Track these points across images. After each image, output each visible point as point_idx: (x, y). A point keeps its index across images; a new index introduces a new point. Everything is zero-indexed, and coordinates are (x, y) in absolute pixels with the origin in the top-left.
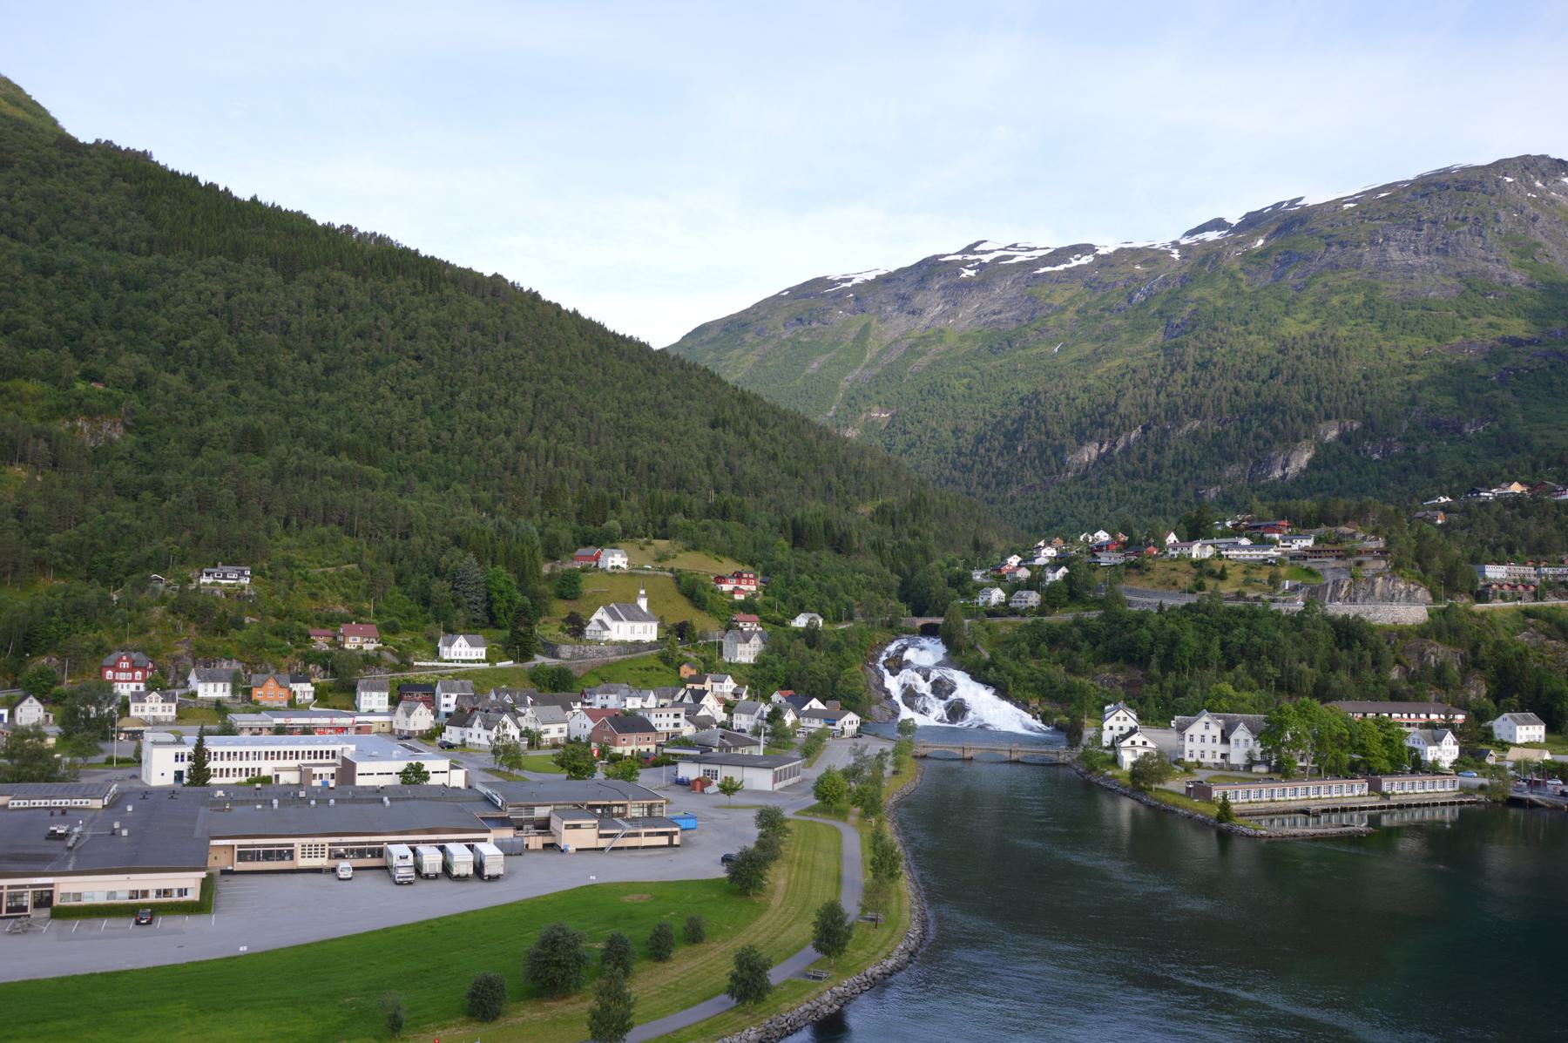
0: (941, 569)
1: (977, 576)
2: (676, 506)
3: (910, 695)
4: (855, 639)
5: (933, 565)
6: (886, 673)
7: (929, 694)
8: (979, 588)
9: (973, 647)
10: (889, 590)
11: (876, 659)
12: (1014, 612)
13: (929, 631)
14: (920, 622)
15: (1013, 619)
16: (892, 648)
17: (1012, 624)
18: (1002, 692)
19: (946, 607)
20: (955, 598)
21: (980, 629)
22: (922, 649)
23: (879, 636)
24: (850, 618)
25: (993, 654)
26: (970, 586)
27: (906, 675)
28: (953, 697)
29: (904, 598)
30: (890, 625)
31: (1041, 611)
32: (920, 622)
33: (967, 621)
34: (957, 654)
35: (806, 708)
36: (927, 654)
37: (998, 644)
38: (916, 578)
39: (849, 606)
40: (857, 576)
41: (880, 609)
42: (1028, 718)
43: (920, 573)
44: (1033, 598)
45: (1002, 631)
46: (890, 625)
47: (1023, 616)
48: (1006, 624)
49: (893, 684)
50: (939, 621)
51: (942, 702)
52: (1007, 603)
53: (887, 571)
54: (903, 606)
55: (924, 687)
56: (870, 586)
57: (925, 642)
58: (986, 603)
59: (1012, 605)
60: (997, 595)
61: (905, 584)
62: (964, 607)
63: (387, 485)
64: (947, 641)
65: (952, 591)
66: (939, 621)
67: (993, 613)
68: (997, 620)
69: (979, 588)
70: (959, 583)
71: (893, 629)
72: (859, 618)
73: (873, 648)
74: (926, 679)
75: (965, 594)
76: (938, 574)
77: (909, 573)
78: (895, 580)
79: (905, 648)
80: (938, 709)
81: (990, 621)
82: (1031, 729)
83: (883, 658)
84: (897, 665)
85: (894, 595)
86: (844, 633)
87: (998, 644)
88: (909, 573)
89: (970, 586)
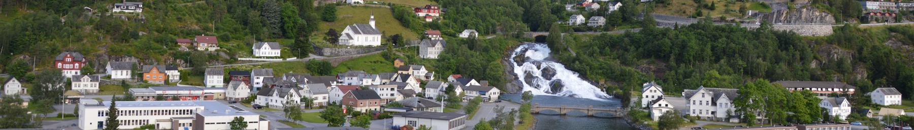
1: (569, 8)
3: (529, 77)
4: (497, 44)
6: (515, 64)
7: (540, 77)
8: (570, 15)
9: (566, 50)
10: (516, 16)
11: (509, 56)
12: (590, 29)
13: (540, 40)
14: (535, 34)
15: (589, 33)
16: (518, 50)
17: (589, 36)
18: (583, 76)
19: (550, 25)
20: (555, 21)
21: (571, 39)
22: (536, 50)
23: (511, 43)
24: (494, 32)
25: (577, 53)
26: (564, 14)
27: (527, 66)
28: (554, 78)
29: (526, 21)
30: (518, 37)
31: (606, 28)
32: (535, 34)
34: (557, 54)
35: (468, 85)
36: (539, 53)
38: (532, 9)
39: (493, 25)
40: (498, 8)
41: (511, 27)
42: (598, 90)
43: (535, 6)
44: (602, 21)
45: (583, 40)
46: (518, 37)
48: (586, 36)
49: (519, 71)
50: (546, 34)
51: (548, 82)
52: (586, 24)
53: (516, 5)
54: (525, 25)
55: (537, 73)
56: (506, 14)
57: (538, 46)
58: (574, 23)
60: (580, 19)
61: (526, 12)
62: (561, 26)
64: (551, 46)
66: (546, 34)
67: (577, 29)
68: (580, 34)
69: (570, 15)
70: (558, 11)
71: (519, 39)
72: (499, 32)
74: (539, 68)
75: (562, 18)
76: (545, 6)
77: (528, 6)
78: (521, 10)
79: (526, 50)
80: (545, 85)
81: (576, 34)
82: (600, 97)
83: (514, 56)
84: (521, 60)
85: (520, 19)
86: (491, 41)
88: (528, 6)
89: (564, 14)
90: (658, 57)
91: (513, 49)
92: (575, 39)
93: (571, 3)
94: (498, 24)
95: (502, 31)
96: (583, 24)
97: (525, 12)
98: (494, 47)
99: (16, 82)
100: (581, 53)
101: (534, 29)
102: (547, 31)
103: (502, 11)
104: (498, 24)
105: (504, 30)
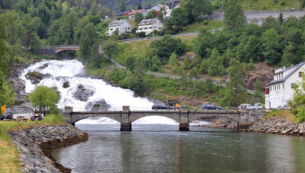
58: (116, 32)
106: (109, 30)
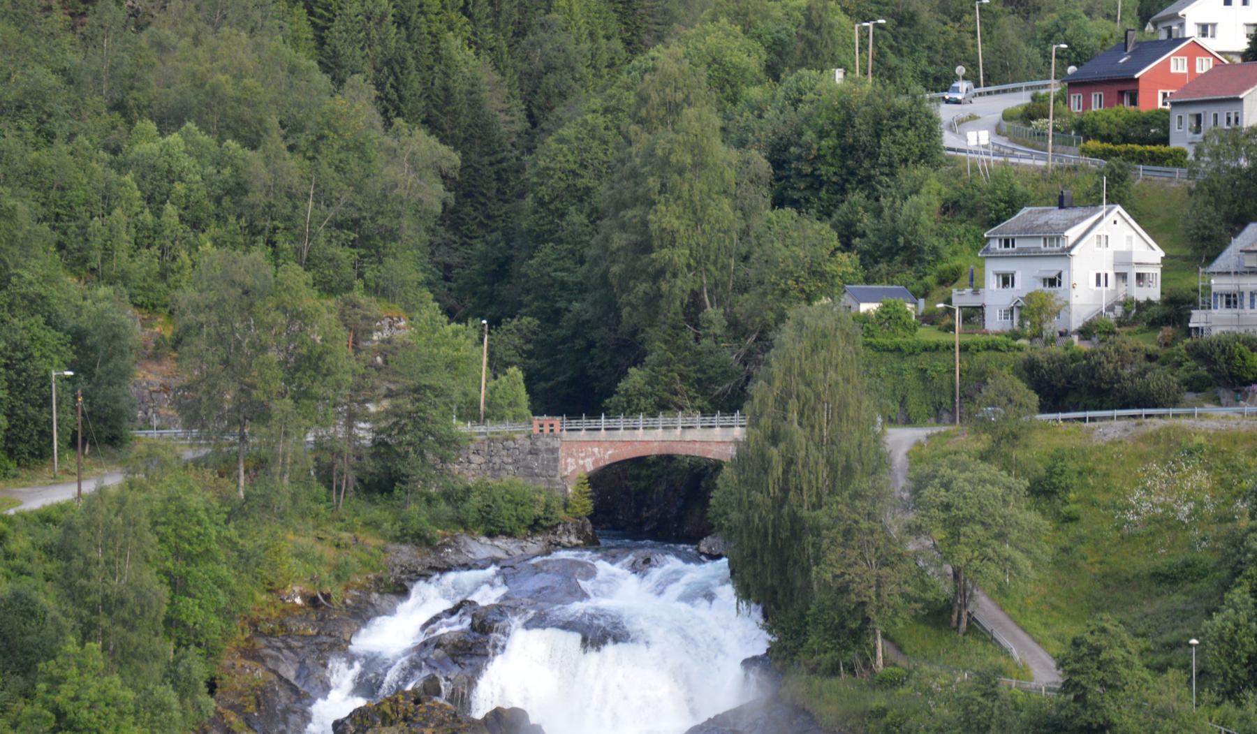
0: (726, 83)
1: (973, 126)
2: (132, 88)
4: (142, 577)
5: (665, 56)
8: (985, 208)
9: (943, 616)
10: (366, 235)
13: (647, 510)
14: (586, 449)
15: (1213, 419)
16: (394, 634)
17: (1215, 454)
19: (756, 338)
20: (818, 280)
21: (996, 488)
22: (599, 634)
23: (304, 552)
24: (103, 433)
25: (1081, 661)
26: (919, 203)
29: (476, 291)
30: (383, 481)
32: (586, 449)
33: (901, 440)
37: (1117, 587)
38: (555, 152)
39: (91, 352)
40: (148, 143)
41: (307, 365)
43: (580, 119)
45: (1144, 502)
46: (383, 481)
47: (484, 568)
48: (1176, 450)
50: (713, 438)
52: (1174, 310)
53: (357, 105)
54: (469, 343)
56: (238, 211)
57: (617, 586)
58: (1033, 311)
59: (1211, 321)
60: (1106, 258)
61: (482, 190)
62: (882, 343)
63: (76, 219)
64: (774, 579)
65: (805, 236)
66: (713, 438)
67: (1072, 382)
68: (1110, 428)
69: (985, 208)
70: (841, 171)
71: (401, 498)
72: (164, 436)
73: (264, 635)
75: (891, 254)
76: (702, 117)
77: (506, 117)
78: (413, 168)
79: (474, 642)
81: (1056, 433)
85: (406, 266)
86: (62, 538)
87: (1117, 587)
88: (506, 117)
89: (919, 203)
90: (1169, 645)
91: (327, 623)
92: (1044, 490)
93: (995, 75)
94: (140, 330)
95: (192, 415)
96: (1136, 314)
97: (464, 187)
98: (98, 614)
99: (1247, 47)
100: (1125, 648)
101: (574, 389)
102: (728, 402)
103: (195, 178)
104: (140, 330)
105: (229, 410)
106: (992, 283)
